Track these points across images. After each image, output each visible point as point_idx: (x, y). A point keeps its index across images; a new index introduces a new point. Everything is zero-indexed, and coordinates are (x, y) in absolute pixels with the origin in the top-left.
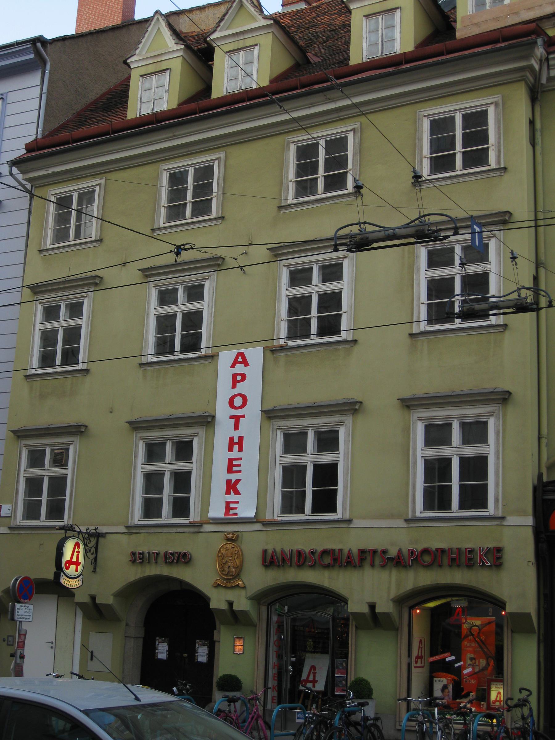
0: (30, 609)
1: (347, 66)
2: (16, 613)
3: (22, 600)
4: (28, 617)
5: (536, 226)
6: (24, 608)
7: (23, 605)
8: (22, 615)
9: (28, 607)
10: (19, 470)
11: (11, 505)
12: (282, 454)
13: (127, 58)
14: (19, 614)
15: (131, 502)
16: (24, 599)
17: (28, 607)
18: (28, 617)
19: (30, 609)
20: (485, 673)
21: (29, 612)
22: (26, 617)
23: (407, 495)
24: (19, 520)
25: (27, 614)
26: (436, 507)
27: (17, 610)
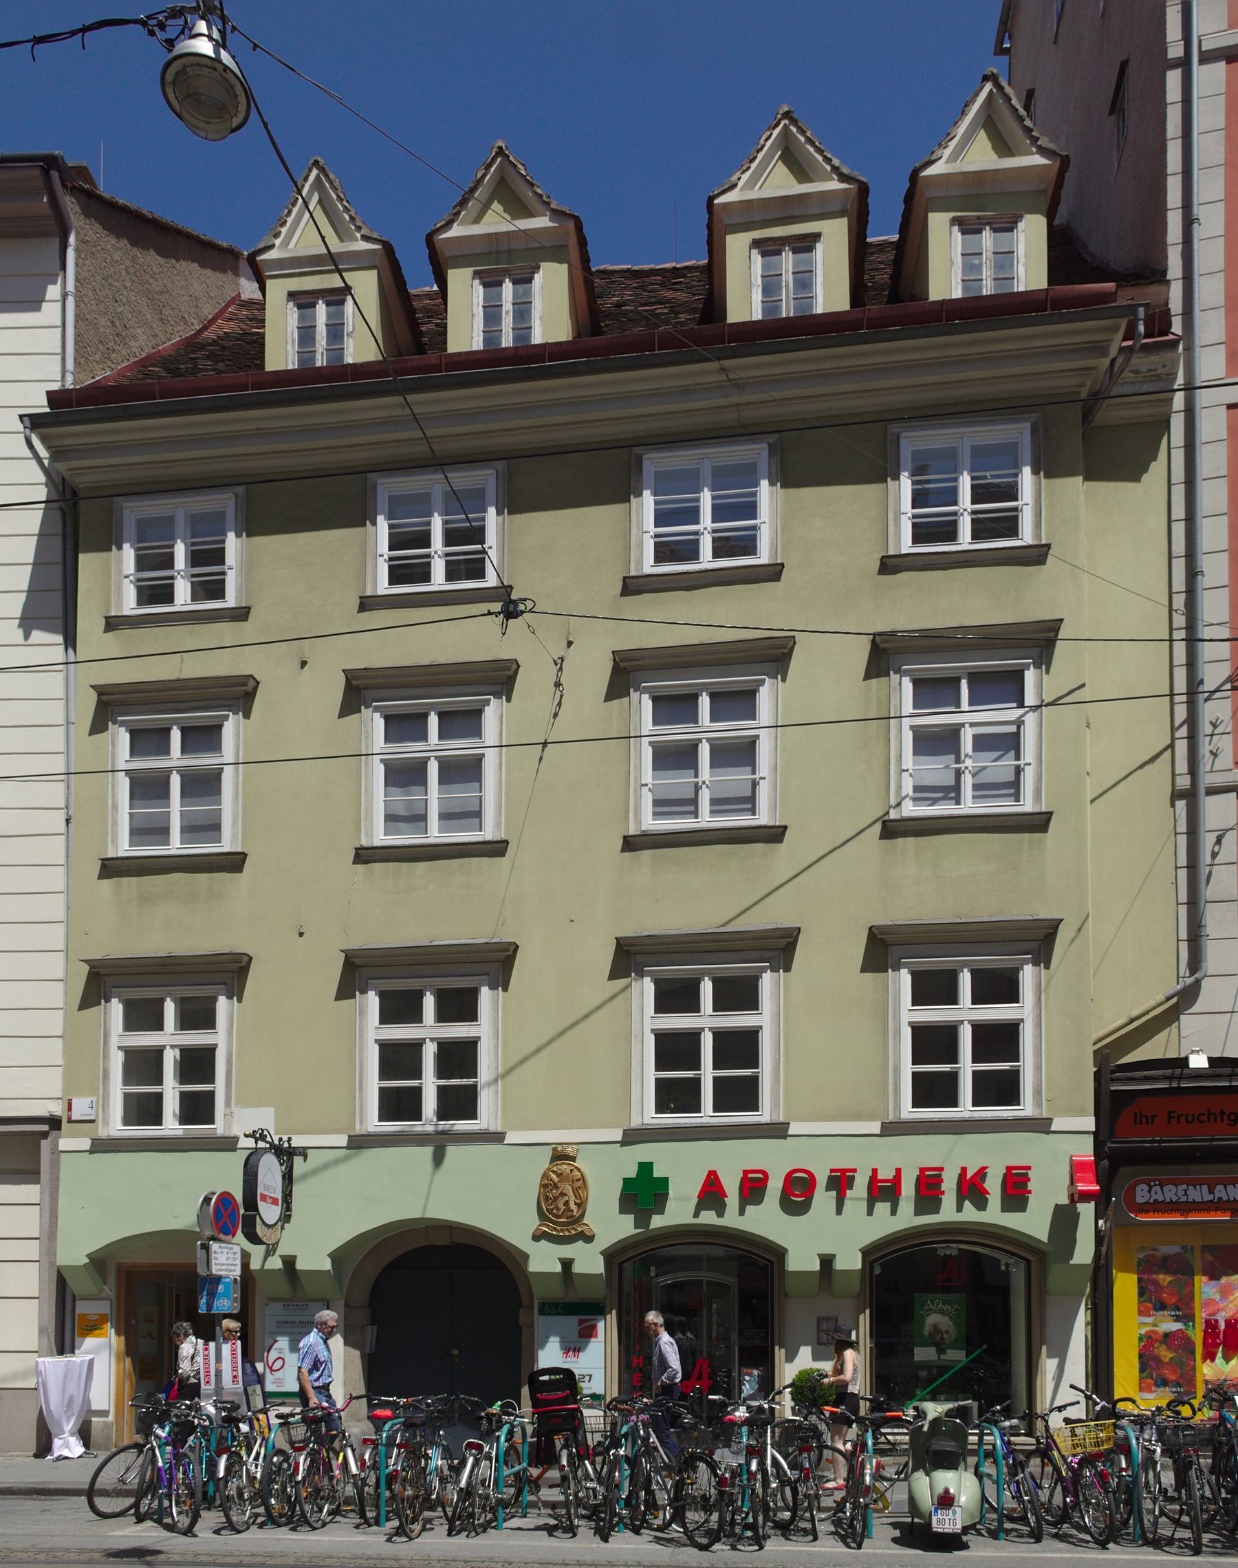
0: (235, 1253)
1: (788, 214)
2: (213, 1262)
3: (222, 1236)
4: (233, 1268)
5: (1171, 640)
6: (225, 1251)
7: (223, 1245)
8: (223, 1265)
9: (232, 1249)
10: (106, 1036)
11: (94, 1099)
12: (1227, 376)
13: (260, 247)
14: (217, 1262)
15: (357, 1094)
16: (224, 1234)
17: (232, 1249)
18: (233, 1268)
19: (235, 1253)
20: (1212, 1414)
21: (235, 1259)
22: (230, 1268)
23: (886, 1082)
24: (116, 1127)
25: (231, 1261)
26: (443, 1082)
27: (213, 1255)
